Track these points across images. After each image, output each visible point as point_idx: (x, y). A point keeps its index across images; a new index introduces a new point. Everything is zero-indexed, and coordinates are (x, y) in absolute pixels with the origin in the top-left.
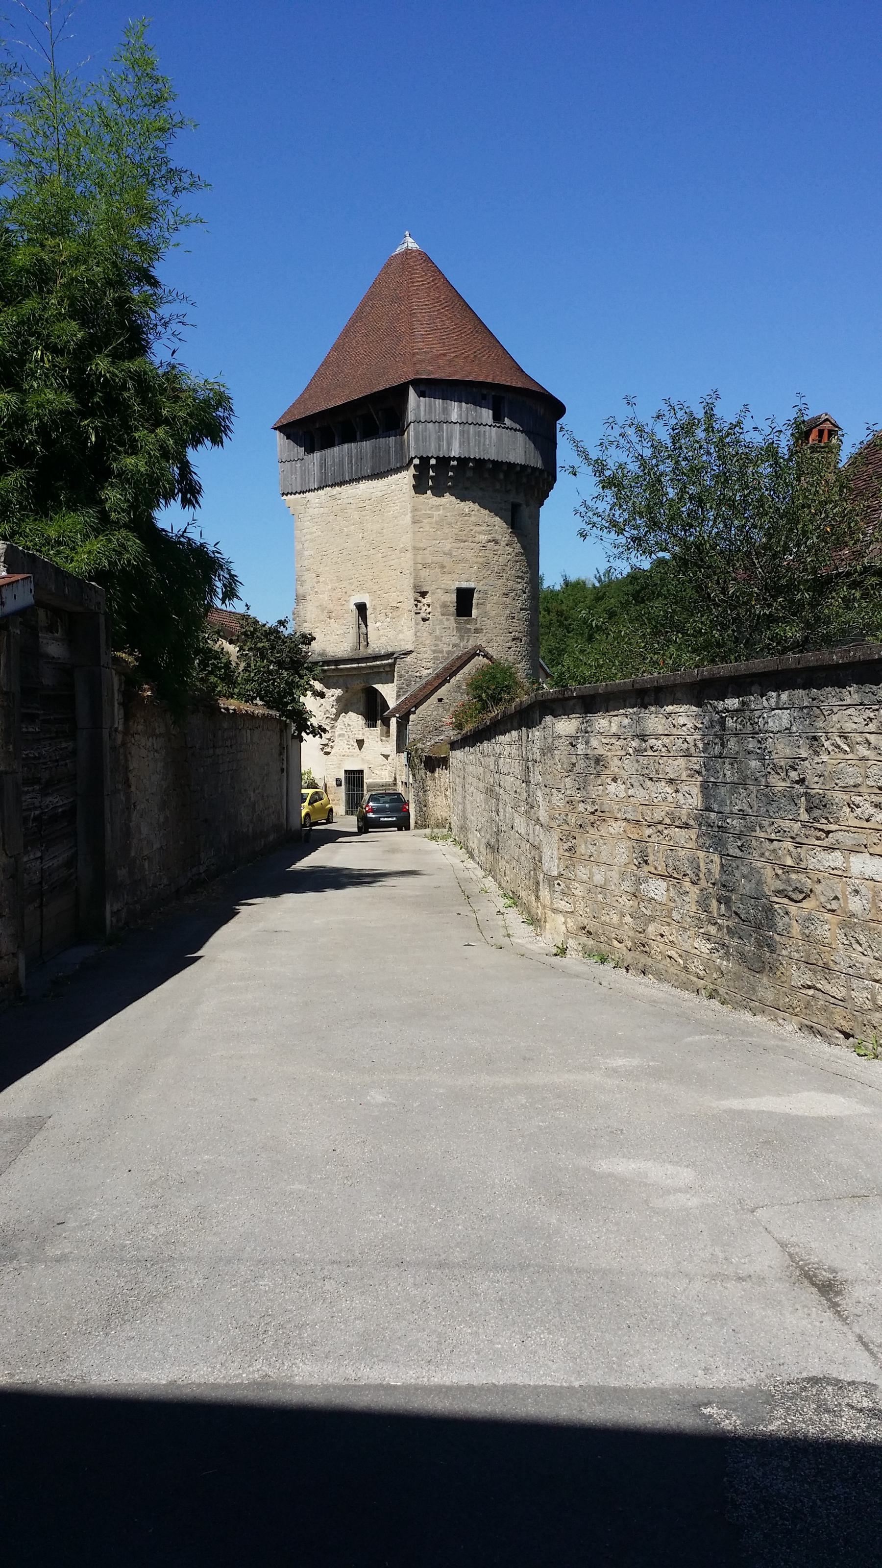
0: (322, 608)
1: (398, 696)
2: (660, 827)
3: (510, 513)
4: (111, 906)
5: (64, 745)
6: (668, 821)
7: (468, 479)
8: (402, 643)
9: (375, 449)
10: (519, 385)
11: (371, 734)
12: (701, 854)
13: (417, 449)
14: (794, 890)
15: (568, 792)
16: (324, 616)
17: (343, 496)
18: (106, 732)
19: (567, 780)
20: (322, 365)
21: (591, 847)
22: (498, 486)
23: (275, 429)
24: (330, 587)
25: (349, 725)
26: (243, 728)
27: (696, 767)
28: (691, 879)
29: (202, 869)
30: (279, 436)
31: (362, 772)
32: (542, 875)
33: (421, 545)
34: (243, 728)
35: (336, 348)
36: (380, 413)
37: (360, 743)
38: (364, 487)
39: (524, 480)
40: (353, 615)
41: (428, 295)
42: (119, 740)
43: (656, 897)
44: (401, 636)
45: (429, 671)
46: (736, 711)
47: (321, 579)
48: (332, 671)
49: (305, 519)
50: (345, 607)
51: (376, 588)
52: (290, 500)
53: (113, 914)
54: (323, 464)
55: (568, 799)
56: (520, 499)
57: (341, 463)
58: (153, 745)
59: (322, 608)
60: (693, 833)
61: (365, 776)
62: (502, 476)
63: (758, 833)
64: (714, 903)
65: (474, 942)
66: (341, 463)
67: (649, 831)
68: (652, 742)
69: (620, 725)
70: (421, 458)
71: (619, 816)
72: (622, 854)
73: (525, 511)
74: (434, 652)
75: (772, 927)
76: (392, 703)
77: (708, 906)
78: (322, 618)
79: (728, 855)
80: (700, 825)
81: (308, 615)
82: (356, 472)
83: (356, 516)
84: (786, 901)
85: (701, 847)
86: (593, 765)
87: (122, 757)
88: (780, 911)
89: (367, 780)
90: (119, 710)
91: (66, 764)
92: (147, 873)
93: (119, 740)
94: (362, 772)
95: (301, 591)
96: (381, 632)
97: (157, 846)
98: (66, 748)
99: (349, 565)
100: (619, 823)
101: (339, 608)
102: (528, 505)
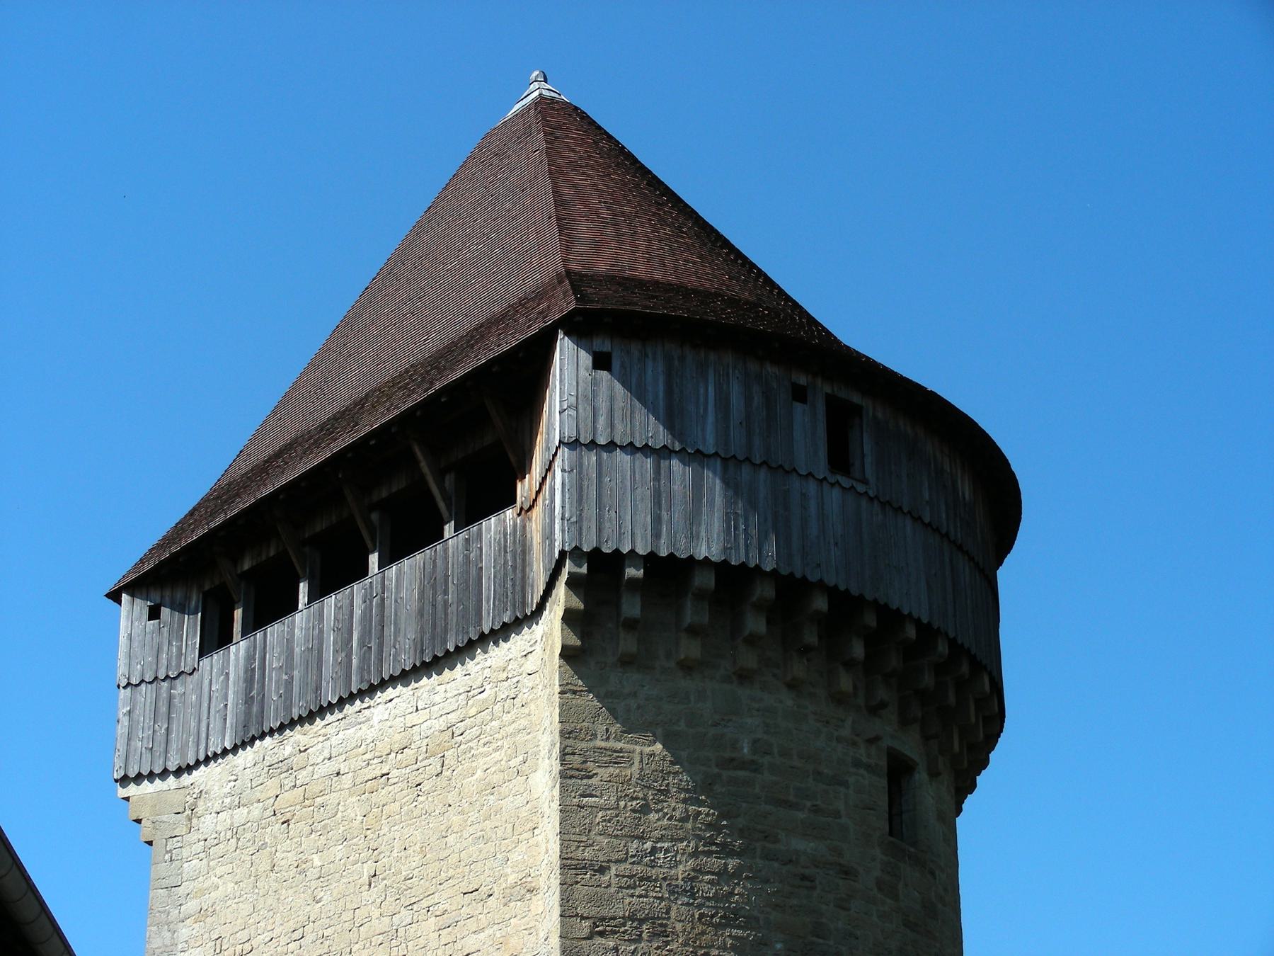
3: (884, 783)
7: (752, 640)
9: (433, 583)
13: (576, 524)
17: (316, 754)
20: (274, 412)
22: (845, 682)
30: (131, 611)
38: (391, 711)
49: (185, 852)
52: (142, 798)
54: (253, 676)
57: (315, 656)
62: (858, 650)
66: (315, 656)
70: (595, 557)
83: (353, 808)
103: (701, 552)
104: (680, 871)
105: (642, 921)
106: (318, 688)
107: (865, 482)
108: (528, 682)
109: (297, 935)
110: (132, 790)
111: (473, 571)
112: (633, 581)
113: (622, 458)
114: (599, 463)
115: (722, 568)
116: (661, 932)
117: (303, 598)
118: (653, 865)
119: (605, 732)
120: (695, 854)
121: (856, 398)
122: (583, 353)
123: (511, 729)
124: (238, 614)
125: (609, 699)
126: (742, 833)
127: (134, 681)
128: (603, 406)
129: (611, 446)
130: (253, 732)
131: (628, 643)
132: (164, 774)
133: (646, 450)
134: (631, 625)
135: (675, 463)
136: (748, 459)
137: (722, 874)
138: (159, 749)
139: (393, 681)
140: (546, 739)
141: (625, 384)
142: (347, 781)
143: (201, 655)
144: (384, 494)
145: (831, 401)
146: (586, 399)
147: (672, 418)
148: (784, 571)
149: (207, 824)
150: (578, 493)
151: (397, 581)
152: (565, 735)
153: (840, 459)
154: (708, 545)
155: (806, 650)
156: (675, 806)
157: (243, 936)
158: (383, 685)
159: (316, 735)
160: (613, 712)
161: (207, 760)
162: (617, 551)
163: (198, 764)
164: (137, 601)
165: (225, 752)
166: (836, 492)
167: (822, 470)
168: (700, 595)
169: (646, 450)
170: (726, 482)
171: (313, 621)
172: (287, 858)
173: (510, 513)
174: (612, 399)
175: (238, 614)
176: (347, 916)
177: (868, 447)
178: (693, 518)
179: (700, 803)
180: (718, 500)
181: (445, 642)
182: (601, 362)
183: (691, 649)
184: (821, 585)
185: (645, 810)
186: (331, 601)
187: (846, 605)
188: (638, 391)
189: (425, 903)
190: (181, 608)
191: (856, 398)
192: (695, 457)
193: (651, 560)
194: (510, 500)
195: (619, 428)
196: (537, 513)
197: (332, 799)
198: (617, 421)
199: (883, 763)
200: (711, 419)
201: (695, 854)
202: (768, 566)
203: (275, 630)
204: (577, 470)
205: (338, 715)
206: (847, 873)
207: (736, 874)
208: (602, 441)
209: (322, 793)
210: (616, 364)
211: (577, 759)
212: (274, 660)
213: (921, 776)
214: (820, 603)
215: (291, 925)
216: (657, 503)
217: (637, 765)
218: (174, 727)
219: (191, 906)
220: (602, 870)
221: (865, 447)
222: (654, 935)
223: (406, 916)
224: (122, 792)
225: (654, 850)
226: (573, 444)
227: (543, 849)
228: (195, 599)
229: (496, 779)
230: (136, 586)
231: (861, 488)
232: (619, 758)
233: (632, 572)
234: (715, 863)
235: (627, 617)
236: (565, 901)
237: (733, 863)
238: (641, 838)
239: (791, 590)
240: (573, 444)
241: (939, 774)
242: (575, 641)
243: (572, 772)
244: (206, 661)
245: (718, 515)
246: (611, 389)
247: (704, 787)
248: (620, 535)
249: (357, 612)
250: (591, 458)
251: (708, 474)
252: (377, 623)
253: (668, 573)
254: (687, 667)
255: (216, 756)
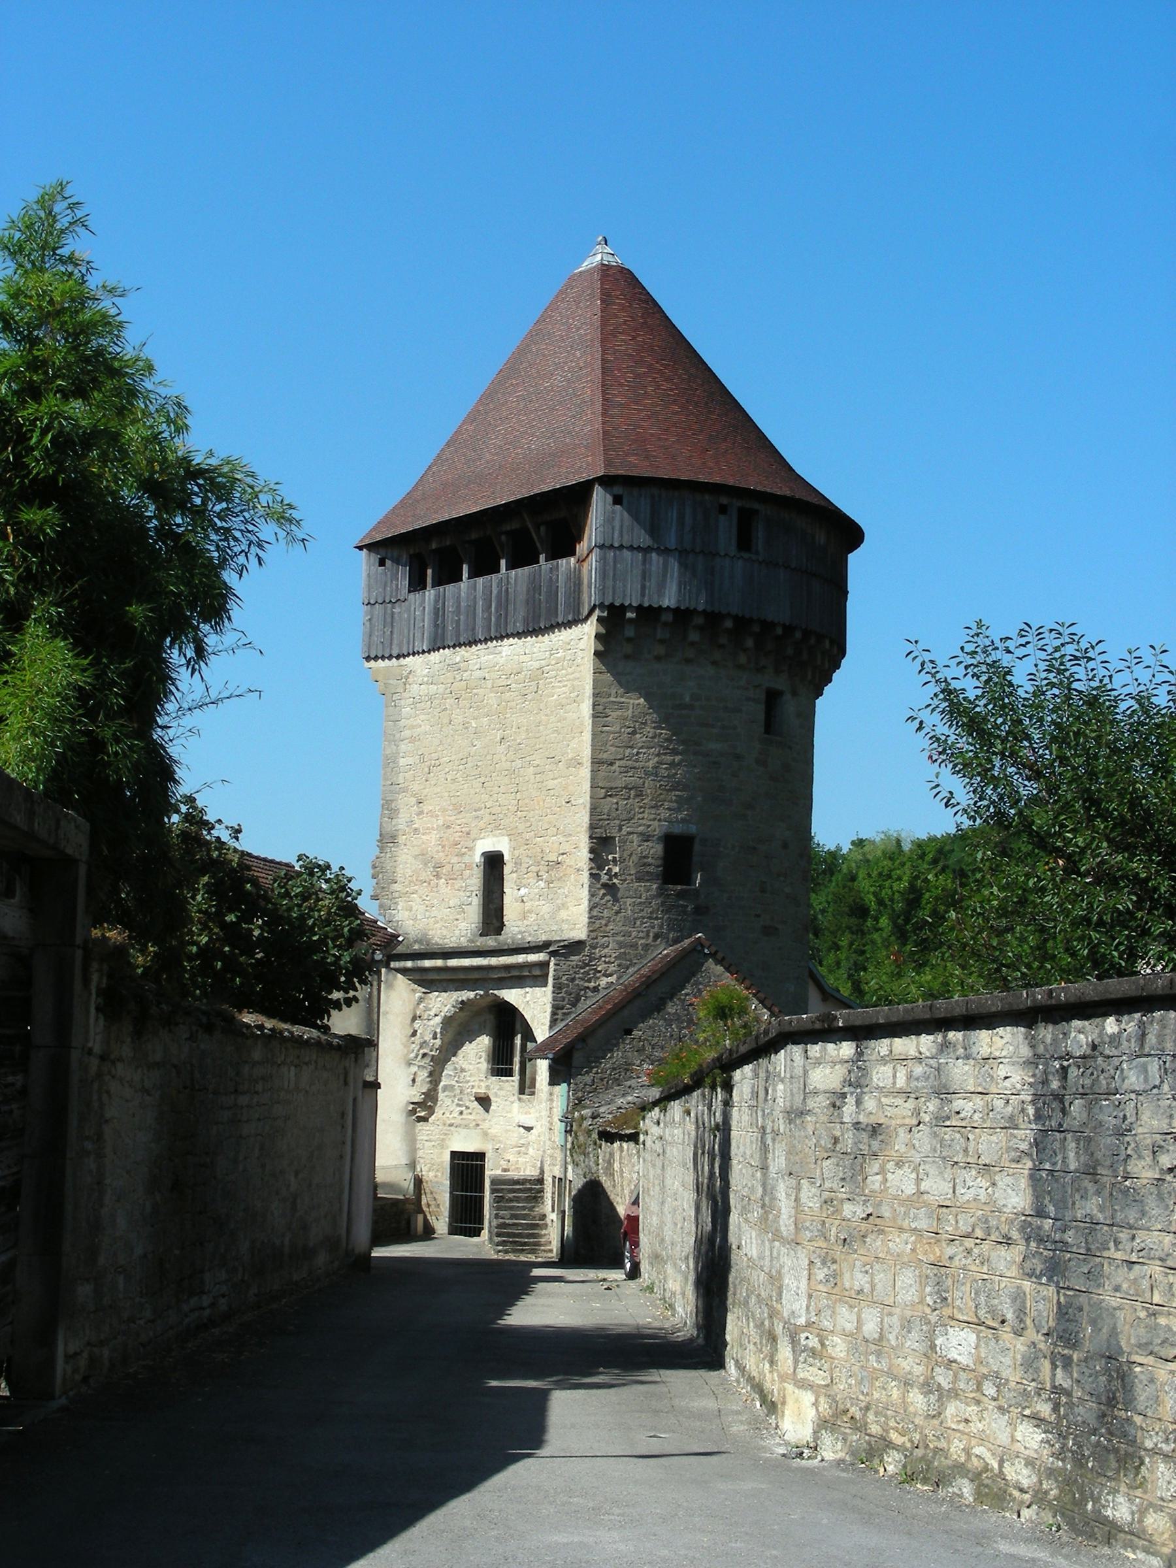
0: (424, 857)
1: (553, 1022)
2: (969, 1243)
3: (762, 707)
4: (66, 1345)
5: (10, 1079)
6: (979, 1233)
7: (692, 644)
8: (565, 927)
9: (534, 586)
10: (786, 492)
11: (501, 1089)
12: (1027, 1285)
13: (602, 591)
14: (1163, 1342)
15: (828, 1185)
16: (427, 874)
18: (75, 1055)
19: (826, 1163)
20: (448, 444)
21: (860, 1276)
22: (743, 659)
23: (360, 548)
24: (440, 822)
25: (463, 1070)
26: (283, 1063)
27: (1024, 1146)
28: (1013, 1327)
29: (206, 1301)
31: (481, 1156)
32: (781, 1325)
33: (605, 756)
34: (283, 1063)
35: (471, 418)
36: (543, 529)
37: (484, 1101)
38: (511, 651)
39: (790, 651)
40: (475, 880)
41: (634, 338)
42: (93, 1070)
43: (959, 1358)
44: (563, 914)
45: (610, 979)
46: (1084, 1057)
47: (426, 808)
48: (433, 970)
50: (466, 859)
51: (521, 827)
52: (378, 670)
53: (68, 1357)
54: (438, 613)
55: (826, 1195)
56: (781, 683)
58: (142, 1081)
59: (424, 857)
60: (1016, 1253)
61: (488, 1164)
62: (750, 643)
63: (1112, 1253)
64: (1046, 1365)
65: (665, 1432)
66: (472, 609)
67: (950, 1251)
68: (958, 1104)
69: (910, 1077)
70: (611, 608)
71: (905, 1224)
72: (908, 1287)
73: (789, 706)
74: (621, 945)
75: (1129, 1404)
76: (542, 1033)
77: (1037, 1370)
78: (424, 876)
79: (1068, 1288)
80: (1028, 1240)
81: (400, 870)
82: (498, 625)
83: (492, 700)
84: (1150, 1360)
85: (1031, 1275)
86: (866, 1140)
87: (95, 1097)
88: (1142, 1377)
89: (492, 1170)
90: (97, 1019)
91: (11, 1111)
92: (121, 1296)
93: (93, 1070)
94: (481, 1156)
95: (388, 828)
96: (528, 906)
97: (139, 1251)
98: (13, 1084)
99: (477, 784)
100: (905, 1236)
101: (454, 860)
102: (795, 693)
103: (666, 603)
104: (651, 764)
105: (630, 789)
106: (473, 629)
107: (757, 553)
108: (580, 653)
109: (463, 762)
110: (372, 664)
111: (554, 588)
112: (631, 620)
113: (627, 554)
114: (615, 556)
115: (677, 611)
116: (640, 795)
117: (465, 575)
118: (637, 761)
119: (615, 693)
120: (658, 755)
121: (756, 506)
122: (608, 496)
123: (571, 677)
124: (494, 1383)
125: (617, 675)
126: (683, 742)
127: (372, 602)
128: (617, 524)
129: (621, 547)
130: (439, 645)
131: (628, 649)
132: (390, 657)
133: (639, 549)
134: (629, 640)
135: (654, 555)
136: (693, 551)
137: (672, 764)
138: (387, 643)
139: (513, 635)
140: (588, 690)
141: (629, 512)
142: (489, 684)
143: (409, 592)
144: (508, 528)
145: (741, 511)
146: (608, 521)
147: (654, 530)
148: (709, 609)
149: (414, 689)
150: (603, 574)
151: (513, 579)
152: (595, 695)
153: (744, 542)
154: (669, 599)
155: (722, 646)
156: (649, 730)
157: (435, 756)
158: (508, 636)
159: (473, 654)
160: (619, 683)
161: (414, 654)
162: (622, 605)
163: (408, 655)
164: (373, 554)
165: (424, 652)
166: (740, 563)
167: (733, 551)
168: (665, 624)
169: (639, 549)
170: (679, 563)
171: (468, 588)
172: (458, 719)
173: (573, 560)
174: (622, 520)
175: (429, 572)
176: (489, 757)
177: (760, 534)
178: (661, 586)
179: (663, 729)
180: (676, 574)
181: (539, 622)
182: (617, 500)
183: (661, 650)
184: (729, 614)
185: (634, 733)
186: (480, 580)
187: (742, 624)
188: (635, 516)
189: (528, 759)
190: (397, 562)
191: (756, 506)
192: (665, 551)
193: (640, 609)
194: (572, 553)
195: (626, 537)
196: (585, 565)
197: (481, 691)
198: (625, 533)
199: (763, 697)
200: (673, 530)
201: (658, 755)
202: (701, 608)
203: (450, 588)
204: (603, 560)
205: (484, 646)
206: (738, 757)
207: (679, 764)
208: (616, 545)
209: (476, 687)
210: (625, 501)
211: (601, 707)
212: (450, 607)
213: (787, 697)
214: (729, 624)
215: (460, 756)
216: (644, 578)
217: (630, 712)
218: (395, 630)
219: (407, 733)
220: (611, 764)
221: (759, 534)
222: (637, 796)
223: (518, 763)
224: (367, 665)
225: (638, 753)
226: (602, 547)
227: (583, 746)
228: (405, 558)
229: (564, 701)
230: (371, 547)
231: (754, 557)
232: (621, 706)
233: (630, 615)
234: (669, 758)
235: (628, 640)
236: (593, 779)
237: (678, 758)
238: (631, 747)
239: (713, 619)
240: (602, 547)
241: (509, 1073)
242: (601, 648)
243: (599, 714)
244: (411, 596)
245: (674, 588)
246: (622, 515)
247: (665, 720)
248: (624, 596)
249: (495, 592)
250: (611, 554)
251: (671, 560)
252: (504, 601)
253: (649, 614)
254: (658, 658)
255: (418, 653)
